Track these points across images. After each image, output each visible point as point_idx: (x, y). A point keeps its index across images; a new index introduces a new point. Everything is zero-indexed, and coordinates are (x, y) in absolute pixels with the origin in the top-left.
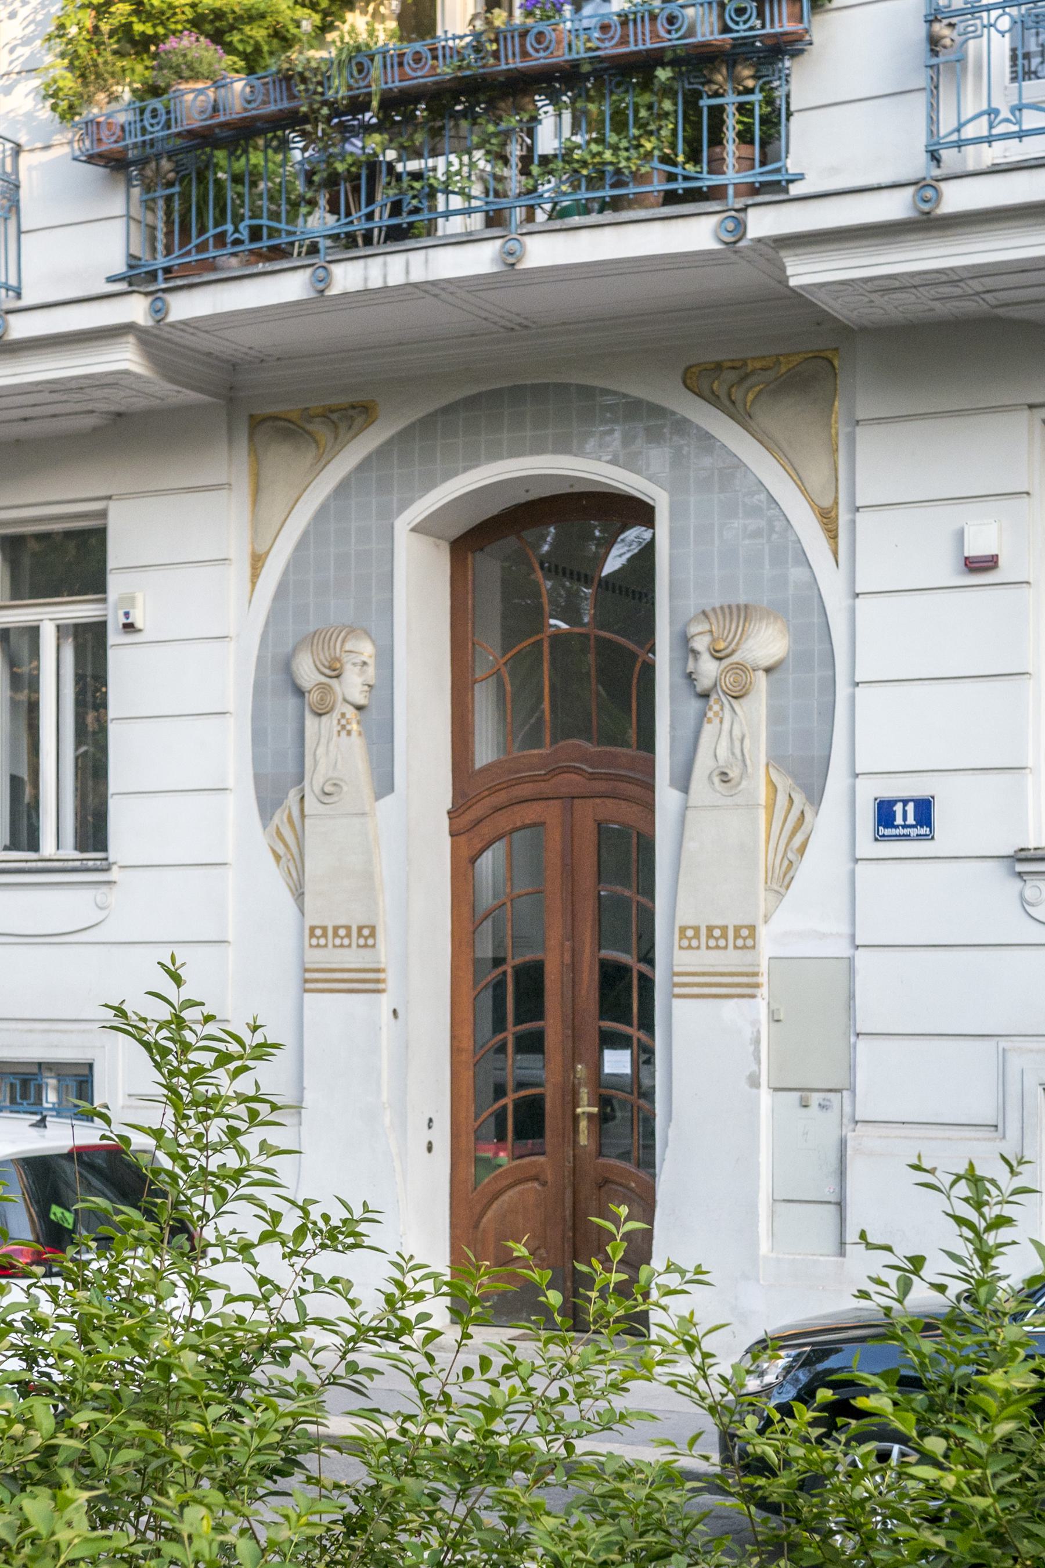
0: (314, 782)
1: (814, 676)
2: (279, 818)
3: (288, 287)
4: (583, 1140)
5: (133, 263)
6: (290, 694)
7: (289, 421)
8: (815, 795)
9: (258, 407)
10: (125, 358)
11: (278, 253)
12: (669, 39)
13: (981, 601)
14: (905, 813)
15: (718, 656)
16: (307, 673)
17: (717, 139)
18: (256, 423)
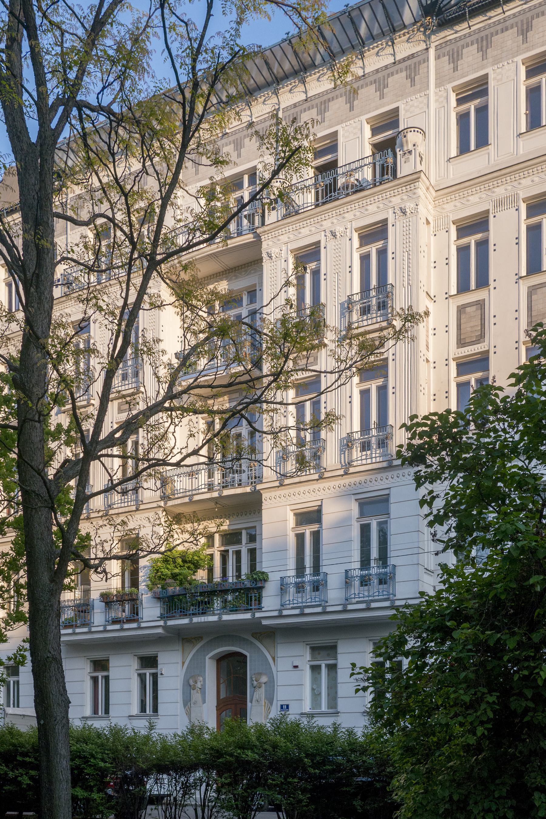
0: (192, 701)
1: (271, 685)
2: (187, 707)
3: (186, 621)
5: (161, 614)
6: (189, 686)
8: (271, 704)
9: (184, 638)
10: (160, 631)
11: (186, 615)
12: (243, 586)
13: (296, 673)
15: (256, 681)
16: (191, 682)
17: (251, 600)
18: (183, 639)
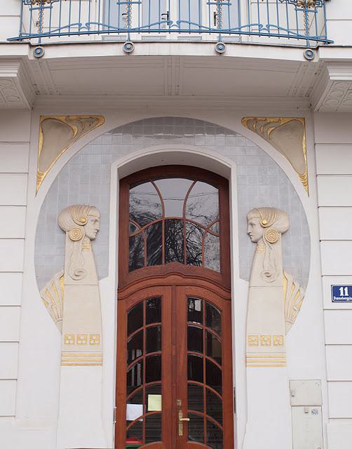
4: (181, 433)
7: (60, 121)
14: (344, 291)
